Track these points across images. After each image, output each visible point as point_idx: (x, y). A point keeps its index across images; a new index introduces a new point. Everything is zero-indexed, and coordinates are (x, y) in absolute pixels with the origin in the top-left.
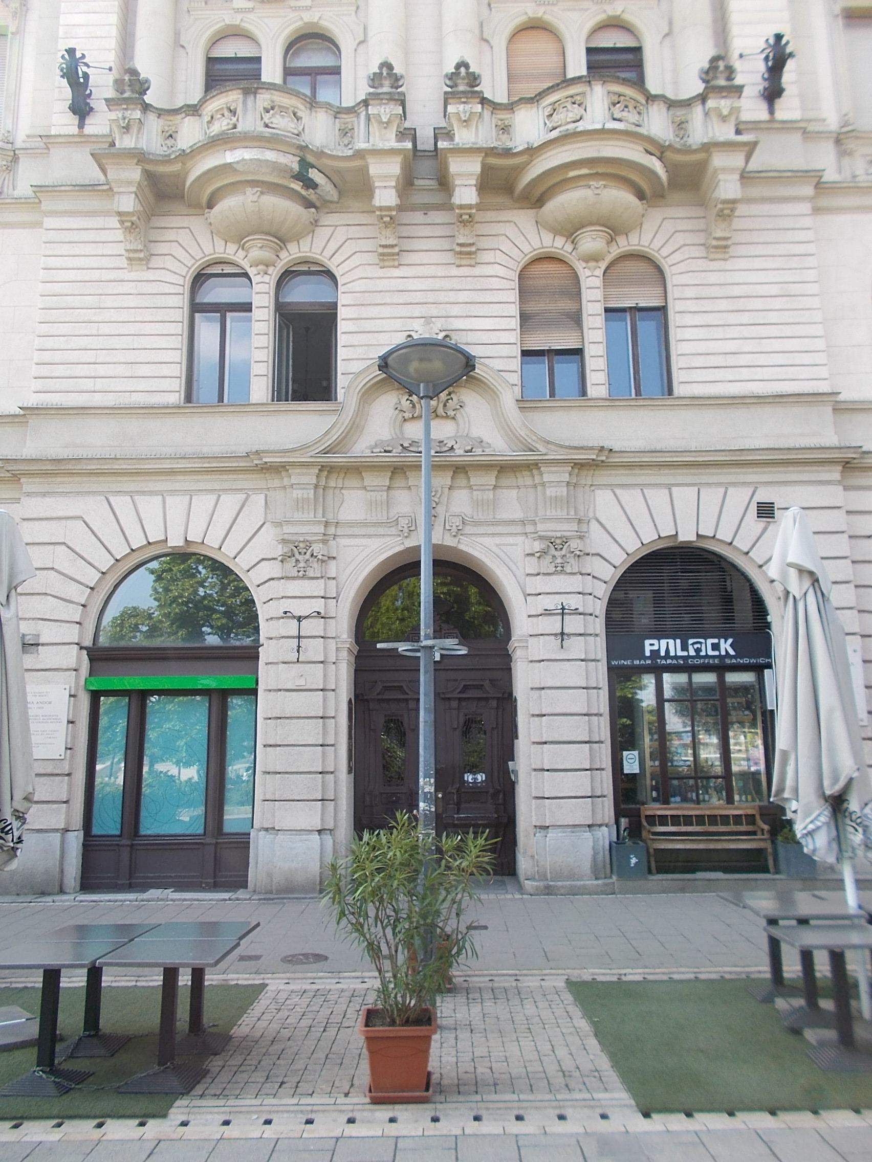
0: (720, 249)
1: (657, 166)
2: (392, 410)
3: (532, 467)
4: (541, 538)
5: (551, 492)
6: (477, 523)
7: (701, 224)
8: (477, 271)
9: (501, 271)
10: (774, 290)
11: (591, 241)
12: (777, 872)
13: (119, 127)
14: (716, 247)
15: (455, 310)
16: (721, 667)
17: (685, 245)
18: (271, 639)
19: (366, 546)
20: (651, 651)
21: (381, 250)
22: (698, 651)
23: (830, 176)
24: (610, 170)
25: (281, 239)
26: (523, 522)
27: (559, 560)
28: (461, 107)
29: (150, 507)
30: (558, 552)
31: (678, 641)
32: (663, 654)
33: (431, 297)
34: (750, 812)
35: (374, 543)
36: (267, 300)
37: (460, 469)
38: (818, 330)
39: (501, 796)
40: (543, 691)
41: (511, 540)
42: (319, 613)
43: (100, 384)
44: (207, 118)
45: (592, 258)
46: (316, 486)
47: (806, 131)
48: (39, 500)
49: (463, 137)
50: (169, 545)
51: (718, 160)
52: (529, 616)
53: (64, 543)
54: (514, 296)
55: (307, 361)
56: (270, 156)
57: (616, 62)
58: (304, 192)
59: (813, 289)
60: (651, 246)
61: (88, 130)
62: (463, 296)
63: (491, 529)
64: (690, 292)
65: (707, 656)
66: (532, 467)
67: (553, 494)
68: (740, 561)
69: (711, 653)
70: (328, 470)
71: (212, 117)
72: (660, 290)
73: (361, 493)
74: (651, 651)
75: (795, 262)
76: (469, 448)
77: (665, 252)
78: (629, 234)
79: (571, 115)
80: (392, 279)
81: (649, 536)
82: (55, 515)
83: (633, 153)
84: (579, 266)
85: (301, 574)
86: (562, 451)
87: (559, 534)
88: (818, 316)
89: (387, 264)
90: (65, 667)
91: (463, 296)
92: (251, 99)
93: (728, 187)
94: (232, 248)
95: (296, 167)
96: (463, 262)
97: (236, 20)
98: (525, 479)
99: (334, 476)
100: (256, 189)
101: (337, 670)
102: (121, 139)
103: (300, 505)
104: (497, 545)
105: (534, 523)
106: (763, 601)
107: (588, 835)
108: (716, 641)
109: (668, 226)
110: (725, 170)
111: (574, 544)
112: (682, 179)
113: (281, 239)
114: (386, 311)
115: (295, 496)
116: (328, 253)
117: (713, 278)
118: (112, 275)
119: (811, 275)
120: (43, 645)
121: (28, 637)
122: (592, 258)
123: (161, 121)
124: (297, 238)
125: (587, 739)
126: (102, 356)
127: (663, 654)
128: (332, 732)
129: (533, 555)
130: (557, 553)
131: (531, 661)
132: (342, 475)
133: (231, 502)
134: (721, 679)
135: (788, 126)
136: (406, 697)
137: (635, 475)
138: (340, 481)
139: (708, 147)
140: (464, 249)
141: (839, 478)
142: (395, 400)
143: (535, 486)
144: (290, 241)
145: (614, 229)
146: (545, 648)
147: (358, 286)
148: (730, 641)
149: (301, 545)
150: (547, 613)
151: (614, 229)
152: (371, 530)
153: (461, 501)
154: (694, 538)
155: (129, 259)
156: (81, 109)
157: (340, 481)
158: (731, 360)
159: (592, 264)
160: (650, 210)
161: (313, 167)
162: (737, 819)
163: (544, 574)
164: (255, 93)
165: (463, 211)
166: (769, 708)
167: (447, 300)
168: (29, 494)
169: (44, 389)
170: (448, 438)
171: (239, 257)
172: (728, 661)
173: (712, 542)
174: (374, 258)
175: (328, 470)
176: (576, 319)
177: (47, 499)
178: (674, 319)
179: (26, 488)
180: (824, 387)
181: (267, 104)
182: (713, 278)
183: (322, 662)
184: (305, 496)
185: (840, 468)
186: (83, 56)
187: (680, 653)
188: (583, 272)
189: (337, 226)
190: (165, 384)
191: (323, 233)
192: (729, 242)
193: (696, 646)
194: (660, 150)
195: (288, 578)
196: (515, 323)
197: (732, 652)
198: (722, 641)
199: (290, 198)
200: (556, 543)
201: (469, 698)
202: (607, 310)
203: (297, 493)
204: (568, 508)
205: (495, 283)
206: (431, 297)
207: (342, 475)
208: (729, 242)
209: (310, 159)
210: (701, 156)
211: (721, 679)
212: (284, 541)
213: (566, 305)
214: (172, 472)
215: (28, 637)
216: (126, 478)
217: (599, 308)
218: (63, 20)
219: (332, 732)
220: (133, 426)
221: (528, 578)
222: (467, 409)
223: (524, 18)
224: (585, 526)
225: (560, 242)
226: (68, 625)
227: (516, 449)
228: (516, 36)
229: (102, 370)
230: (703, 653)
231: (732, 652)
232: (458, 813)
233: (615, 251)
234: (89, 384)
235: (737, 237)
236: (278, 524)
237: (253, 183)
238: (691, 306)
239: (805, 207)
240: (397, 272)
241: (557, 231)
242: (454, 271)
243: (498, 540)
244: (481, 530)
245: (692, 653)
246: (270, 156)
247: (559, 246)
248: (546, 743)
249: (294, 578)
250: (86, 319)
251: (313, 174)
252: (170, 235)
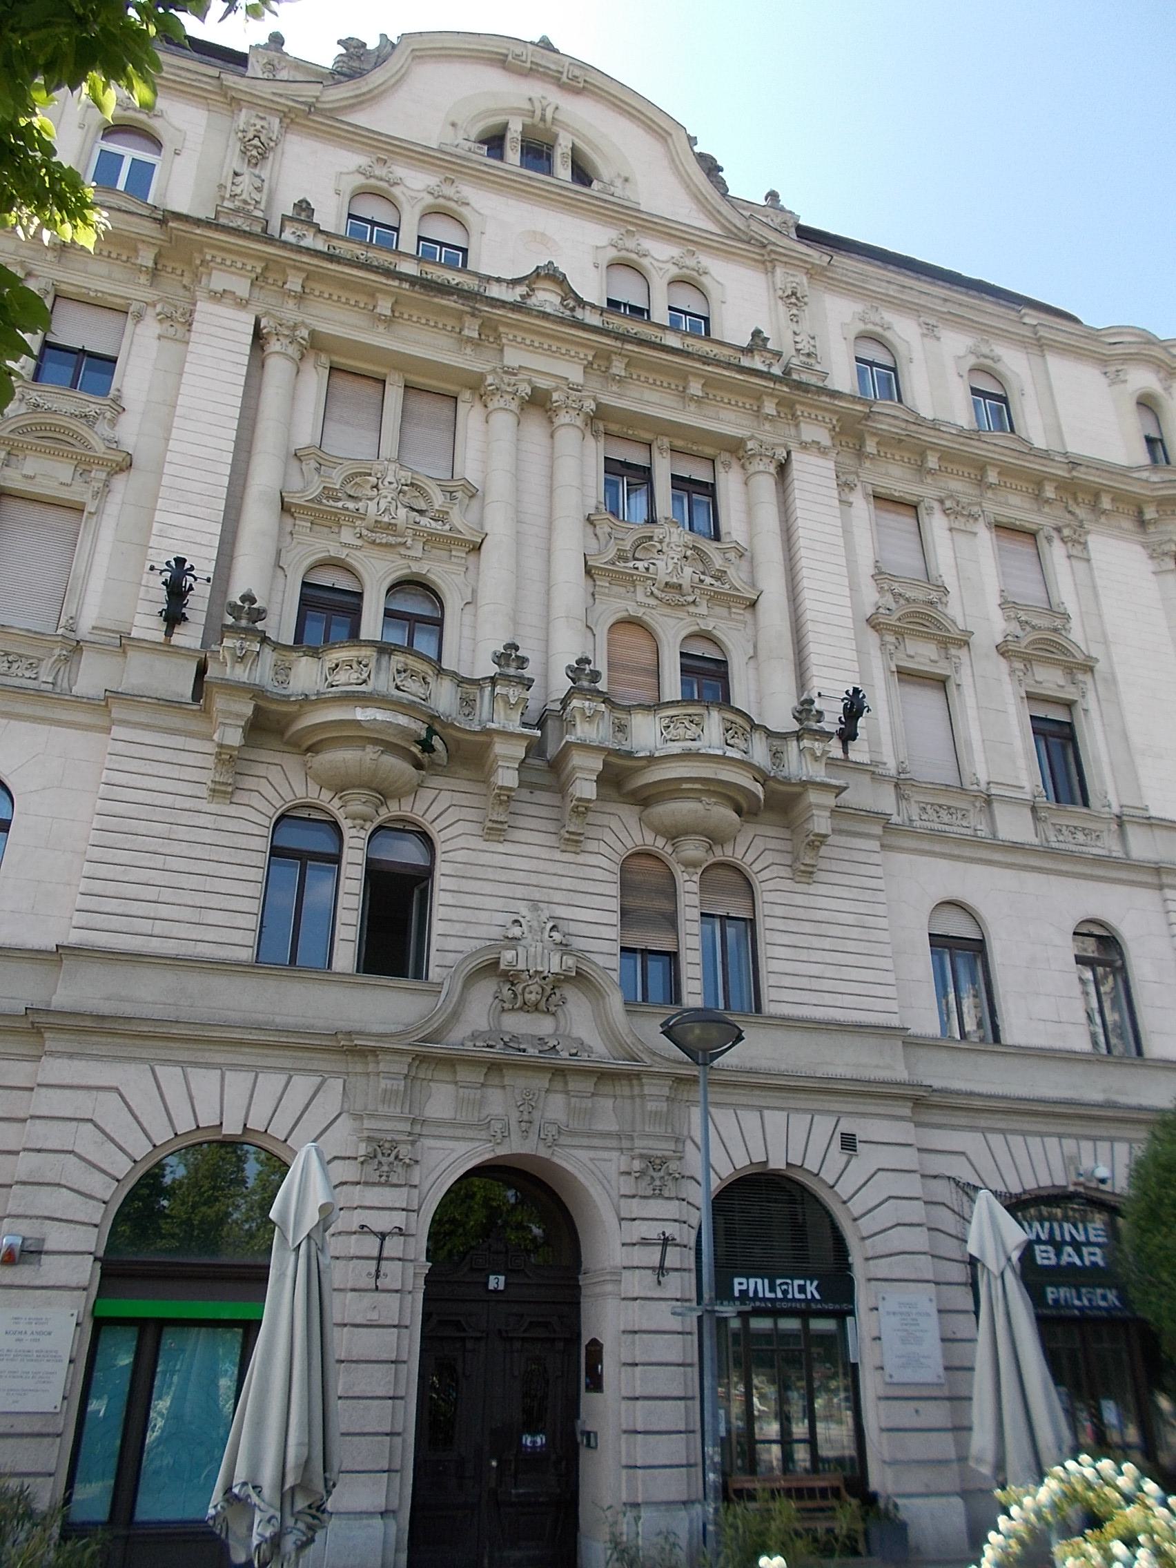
0: (806, 874)
1: (759, 790)
2: (491, 999)
3: (632, 1077)
4: (642, 1156)
5: (651, 1106)
6: (572, 1133)
7: (787, 846)
8: (581, 859)
9: (605, 863)
10: (850, 919)
11: (693, 849)
12: (870, 1553)
13: (234, 655)
14: (803, 872)
15: (558, 897)
16: (805, 1312)
18: (338, 1258)
19: (453, 1150)
20: (740, 1291)
21: (490, 825)
22: (785, 1292)
23: (895, 819)
24: (724, 791)
25: (384, 794)
26: (619, 1136)
27: (658, 1183)
28: (587, 703)
29: (205, 1082)
30: (657, 1174)
31: (766, 1281)
32: (751, 1294)
33: (534, 879)
34: (836, 1483)
35: (461, 1147)
37: (559, 1072)
38: (887, 964)
39: (564, 1463)
40: (637, 1336)
41: (605, 1155)
42: (400, 1229)
43: (159, 928)
44: (328, 665)
45: (690, 864)
46: (406, 1077)
47: (872, 771)
48: (65, 1062)
49: (584, 731)
50: (224, 1132)
51: (813, 797)
52: (623, 1245)
53: (91, 1120)
54: (615, 890)
55: (395, 925)
56: (402, 720)
57: (708, 676)
58: (419, 755)
59: (883, 923)
61: (176, 639)
62: (566, 883)
63: (585, 1142)
64: (779, 911)
65: (794, 1299)
66: (632, 1077)
67: (654, 1108)
68: (824, 1194)
69: (797, 1296)
70: (421, 1059)
71: (337, 666)
72: (748, 903)
73: (451, 1087)
74: (740, 1291)
75: (867, 895)
76: (574, 1051)
79: (689, 732)
80: (495, 854)
81: (742, 1162)
82: (83, 1083)
83: (743, 779)
84: (678, 870)
85: (383, 1179)
86: (668, 1064)
87: (659, 1153)
88: (888, 950)
90: (74, 1285)
91: (566, 883)
92: (385, 659)
93: (821, 823)
94: (326, 795)
95: (424, 734)
96: (569, 848)
97: (343, 554)
98: (624, 1089)
99: (425, 1065)
100: (378, 748)
101: (413, 1300)
102: (233, 667)
104: (591, 1160)
105: (631, 1138)
106: (844, 1240)
107: (683, 1514)
108: (802, 1282)
109: (759, 843)
110: (819, 806)
111: (673, 1166)
112: (777, 804)
113: (384, 794)
114: (488, 888)
115: (383, 1086)
117: (799, 899)
118: (189, 803)
119: (880, 909)
120: (47, 1253)
121: (29, 1242)
122: (690, 864)
123: (275, 654)
125: (682, 1395)
126: (167, 895)
127: (751, 1294)
128: (403, 1382)
129: (629, 1173)
130: (655, 1174)
131: (624, 1299)
133: (303, 1085)
134: (805, 1325)
135: (858, 767)
136: (463, 1334)
137: (728, 1094)
138: (429, 1073)
139: (806, 784)
140: (573, 837)
141: (910, 1115)
142: (495, 988)
143: (632, 1097)
144: (392, 797)
146: (638, 1283)
147: (460, 856)
148: (815, 1283)
149: (387, 1145)
150: (645, 1242)
151: (714, 838)
152: (459, 1132)
153: (555, 1107)
154: (783, 1167)
156: (174, 617)
157: (429, 1073)
158: (815, 984)
159: (691, 870)
160: (746, 825)
161: (437, 734)
162: (823, 1492)
163: (642, 1197)
164: (390, 654)
166: (852, 1361)
167: (550, 884)
168: (51, 1054)
169: (89, 926)
170: (549, 1036)
171: (334, 806)
172: (813, 1306)
173: (800, 1171)
175: (421, 1059)
176: (671, 921)
177: (76, 1062)
178: (763, 936)
179: (49, 1046)
180: (895, 1021)
181: (400, 666)
182: (799, 899)
183: (397, 1291)
184: (395, 1087)
186: (192, 568)
187: (768, 1295)
188: (681, 875)
190: (237, 937)
193: (784, 1287)
194: (763, 777)
195: (366, 1183)
196: (615, 918)
197: (817, 1296)
198: (808, 1283)
199: (404, 759)
200: (654, 1163)
201: (532, 1339)
202: (702, 915)
203: (384, 1084)
205: (598, 874)
206: (534, 879)
209: (437, 727)
210: (797, 789)
211: (805, 1325)
212: (369, 1139)
213: (663, 905)
214: (241, 1043)
215: (29, 1242)
216: (178, 1045)
217: (695, 914)
218: (158, 516)
219: (403, 1382)
220: (194, 982)
221: (623, 1201)
222: (569, 1006)
223: (625, 614)
224: (680, 1145)
225: (660, 842)
226: (84, 1228)
227: (616, 1055)
228: (949, 907)
229: (164, 911)
230: (790, 1296)
231: (817, 1296)
232: (516, 1486)
234: (146, 926)
235: (823, 864)
236: (358, 1117)
237: (375, 742)
238: (779, 924)
239: (875, 845)
240: (500, 848)
241: (658, 832)
242: (558, 856)
243: (592, 1154)
244: (576, 1141)
245: (780, 1295)
246: (402, 720)
247: (659, 844)
248: (637, 1399)
249: (374, 1184)
250: (151, 849)
251: (436, 742)
252: (260, 770)
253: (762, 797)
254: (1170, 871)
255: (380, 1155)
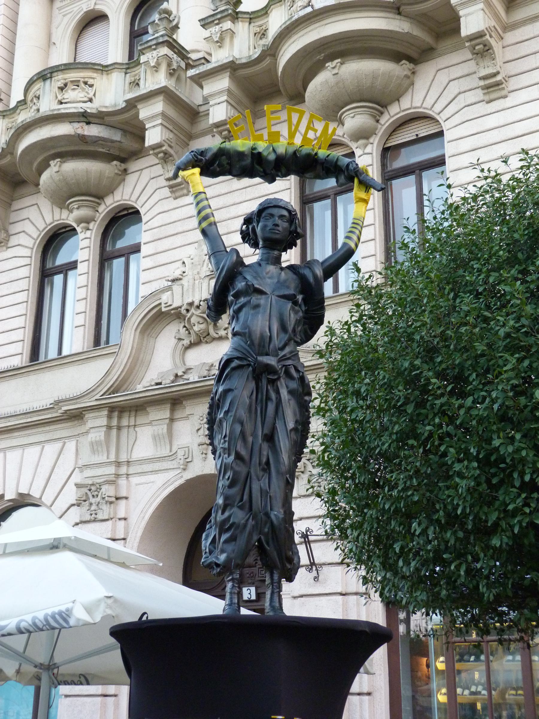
2: (174, 341)
17: (460, 93)
35: (160, 479)
36: (87, 254)
45: (362, 135)
46: (109, 427)
60: (424, 106)
77: (438, 108)
78: (401, 99)
89: (178, 194)
99: (126, 414)
103: (95, 447)
113: (96, 194)
114: (178, 241)
116: (134, 198)
124: (111, 191)
132: (133, 413)
145: (378, 100)
149: (93, 488)
155: (170, 187)
165: (474, 42)
167: (228, 216)
174: (479, 94)
175: (112, 409)
184: (98, 439)
185: (168, 406)
189: (142, 170)
191: (131, 179)
192: (499, 78)
204: (108, 452)
207: (133, 413)
208: (499, 78)
233: (387, 120)
252: (24, 214)
253: (417, 32)
254: (310, 2)
255: (91, 497)
